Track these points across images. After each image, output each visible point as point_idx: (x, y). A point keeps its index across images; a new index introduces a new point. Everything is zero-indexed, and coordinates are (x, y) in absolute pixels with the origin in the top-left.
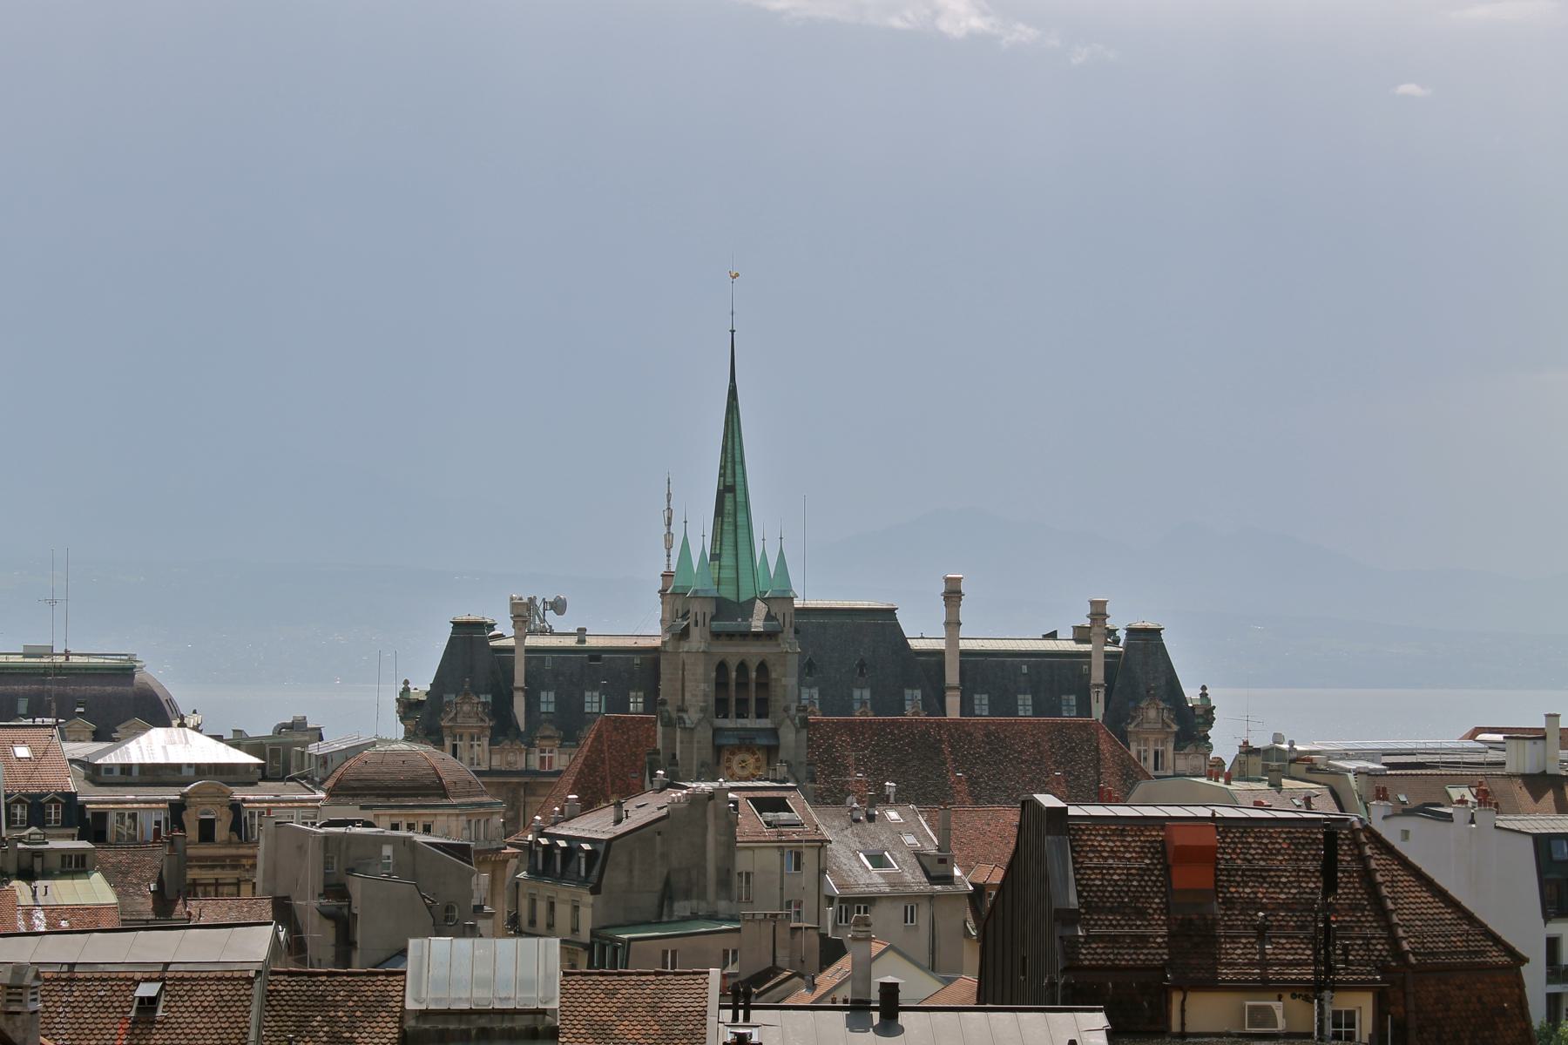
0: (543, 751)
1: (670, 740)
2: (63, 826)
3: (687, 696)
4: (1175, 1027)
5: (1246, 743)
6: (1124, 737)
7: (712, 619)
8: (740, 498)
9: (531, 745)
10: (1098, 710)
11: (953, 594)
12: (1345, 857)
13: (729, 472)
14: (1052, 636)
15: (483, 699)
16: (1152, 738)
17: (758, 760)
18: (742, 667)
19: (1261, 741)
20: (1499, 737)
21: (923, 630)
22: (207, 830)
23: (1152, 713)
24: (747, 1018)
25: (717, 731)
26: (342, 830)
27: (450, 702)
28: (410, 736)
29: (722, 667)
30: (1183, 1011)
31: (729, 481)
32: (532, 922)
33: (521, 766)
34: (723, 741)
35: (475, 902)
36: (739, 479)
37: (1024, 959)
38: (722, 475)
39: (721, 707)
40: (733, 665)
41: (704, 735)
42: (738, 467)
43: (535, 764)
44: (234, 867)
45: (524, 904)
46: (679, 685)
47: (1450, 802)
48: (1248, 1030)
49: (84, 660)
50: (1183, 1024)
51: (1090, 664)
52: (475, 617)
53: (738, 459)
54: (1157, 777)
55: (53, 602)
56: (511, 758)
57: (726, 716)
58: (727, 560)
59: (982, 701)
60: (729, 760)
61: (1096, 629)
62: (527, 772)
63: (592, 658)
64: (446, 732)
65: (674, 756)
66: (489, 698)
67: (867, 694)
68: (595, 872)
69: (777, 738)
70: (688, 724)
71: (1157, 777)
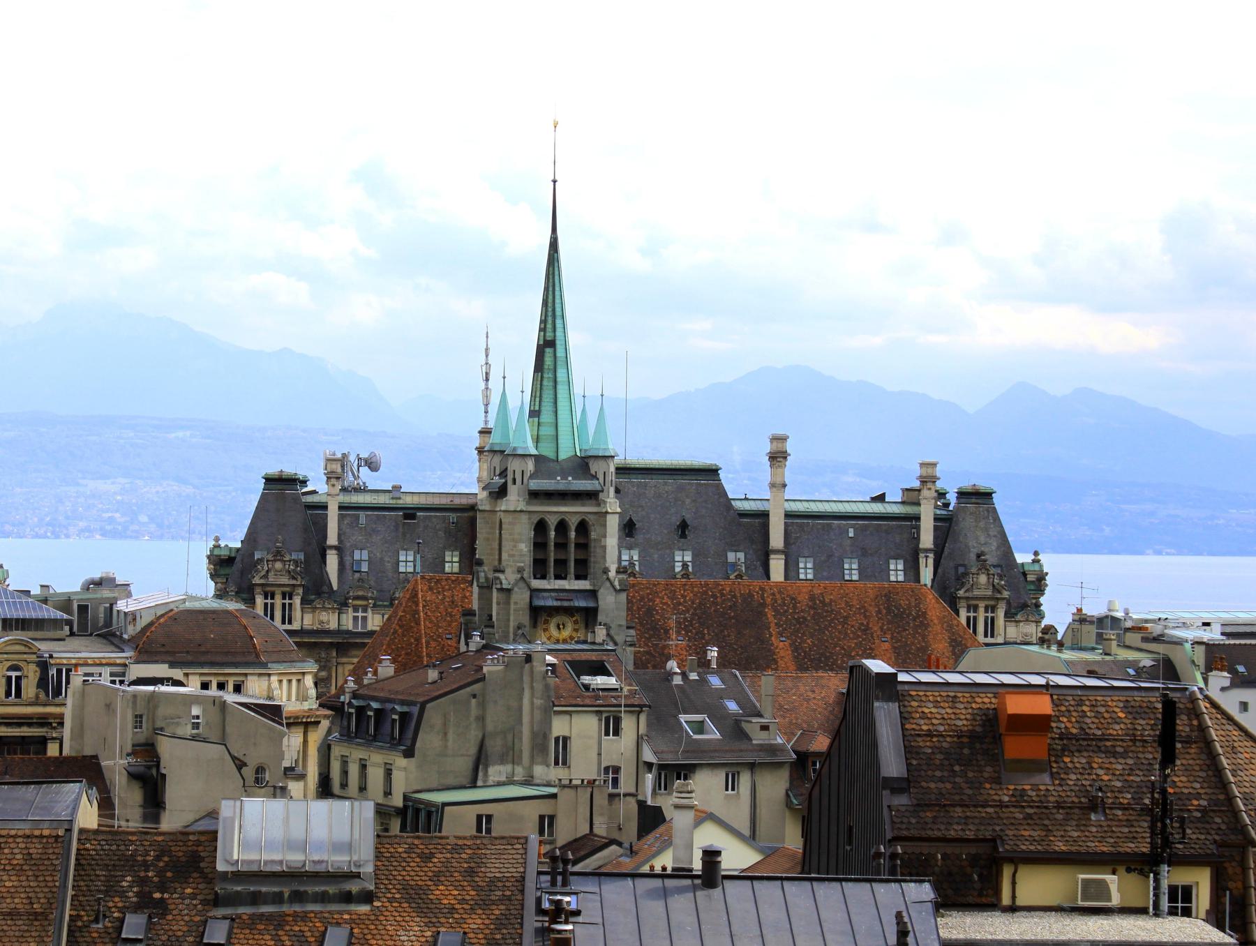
3: (505, 556)
5: (1079, 610)
7: (531, 477)
8: (560, 353)
10: (927, 575)
17: (576, 622)
18: (562, 526)
19: (1094, 609)
21: (745, 484)
24: (565, 884)
26: (151, 688)
28: (220, 595)
29: (541, 527)
30: (1014, 883)
31: (549, 335)
32: (344, 785)
33: (333, 625)
34: (541, 603)
35: (286, 763)
36: (559, 333)
37: (850, 828)
38: (543, 329)
39: (540, 568)
40: (552, 522)
41: (521, 598)
43: (348, 622)
44: (42, 725)
46: (496, 546)
48: (1080, 903)
50: (1014, 897)
51: (918, 528)
52: (289, 469)
53: (558, 313)
56: (324, 616)
57: (543, 577)
58: (546, 416)
59: (806, 570)
60: (546, 622)
61: (925, 493)
62: (338, 632)
63: (407, 516)
64: (258, 590)
65: (490, 616)
66: (302, 557)
68: (410, 734)
71: (987, 645)
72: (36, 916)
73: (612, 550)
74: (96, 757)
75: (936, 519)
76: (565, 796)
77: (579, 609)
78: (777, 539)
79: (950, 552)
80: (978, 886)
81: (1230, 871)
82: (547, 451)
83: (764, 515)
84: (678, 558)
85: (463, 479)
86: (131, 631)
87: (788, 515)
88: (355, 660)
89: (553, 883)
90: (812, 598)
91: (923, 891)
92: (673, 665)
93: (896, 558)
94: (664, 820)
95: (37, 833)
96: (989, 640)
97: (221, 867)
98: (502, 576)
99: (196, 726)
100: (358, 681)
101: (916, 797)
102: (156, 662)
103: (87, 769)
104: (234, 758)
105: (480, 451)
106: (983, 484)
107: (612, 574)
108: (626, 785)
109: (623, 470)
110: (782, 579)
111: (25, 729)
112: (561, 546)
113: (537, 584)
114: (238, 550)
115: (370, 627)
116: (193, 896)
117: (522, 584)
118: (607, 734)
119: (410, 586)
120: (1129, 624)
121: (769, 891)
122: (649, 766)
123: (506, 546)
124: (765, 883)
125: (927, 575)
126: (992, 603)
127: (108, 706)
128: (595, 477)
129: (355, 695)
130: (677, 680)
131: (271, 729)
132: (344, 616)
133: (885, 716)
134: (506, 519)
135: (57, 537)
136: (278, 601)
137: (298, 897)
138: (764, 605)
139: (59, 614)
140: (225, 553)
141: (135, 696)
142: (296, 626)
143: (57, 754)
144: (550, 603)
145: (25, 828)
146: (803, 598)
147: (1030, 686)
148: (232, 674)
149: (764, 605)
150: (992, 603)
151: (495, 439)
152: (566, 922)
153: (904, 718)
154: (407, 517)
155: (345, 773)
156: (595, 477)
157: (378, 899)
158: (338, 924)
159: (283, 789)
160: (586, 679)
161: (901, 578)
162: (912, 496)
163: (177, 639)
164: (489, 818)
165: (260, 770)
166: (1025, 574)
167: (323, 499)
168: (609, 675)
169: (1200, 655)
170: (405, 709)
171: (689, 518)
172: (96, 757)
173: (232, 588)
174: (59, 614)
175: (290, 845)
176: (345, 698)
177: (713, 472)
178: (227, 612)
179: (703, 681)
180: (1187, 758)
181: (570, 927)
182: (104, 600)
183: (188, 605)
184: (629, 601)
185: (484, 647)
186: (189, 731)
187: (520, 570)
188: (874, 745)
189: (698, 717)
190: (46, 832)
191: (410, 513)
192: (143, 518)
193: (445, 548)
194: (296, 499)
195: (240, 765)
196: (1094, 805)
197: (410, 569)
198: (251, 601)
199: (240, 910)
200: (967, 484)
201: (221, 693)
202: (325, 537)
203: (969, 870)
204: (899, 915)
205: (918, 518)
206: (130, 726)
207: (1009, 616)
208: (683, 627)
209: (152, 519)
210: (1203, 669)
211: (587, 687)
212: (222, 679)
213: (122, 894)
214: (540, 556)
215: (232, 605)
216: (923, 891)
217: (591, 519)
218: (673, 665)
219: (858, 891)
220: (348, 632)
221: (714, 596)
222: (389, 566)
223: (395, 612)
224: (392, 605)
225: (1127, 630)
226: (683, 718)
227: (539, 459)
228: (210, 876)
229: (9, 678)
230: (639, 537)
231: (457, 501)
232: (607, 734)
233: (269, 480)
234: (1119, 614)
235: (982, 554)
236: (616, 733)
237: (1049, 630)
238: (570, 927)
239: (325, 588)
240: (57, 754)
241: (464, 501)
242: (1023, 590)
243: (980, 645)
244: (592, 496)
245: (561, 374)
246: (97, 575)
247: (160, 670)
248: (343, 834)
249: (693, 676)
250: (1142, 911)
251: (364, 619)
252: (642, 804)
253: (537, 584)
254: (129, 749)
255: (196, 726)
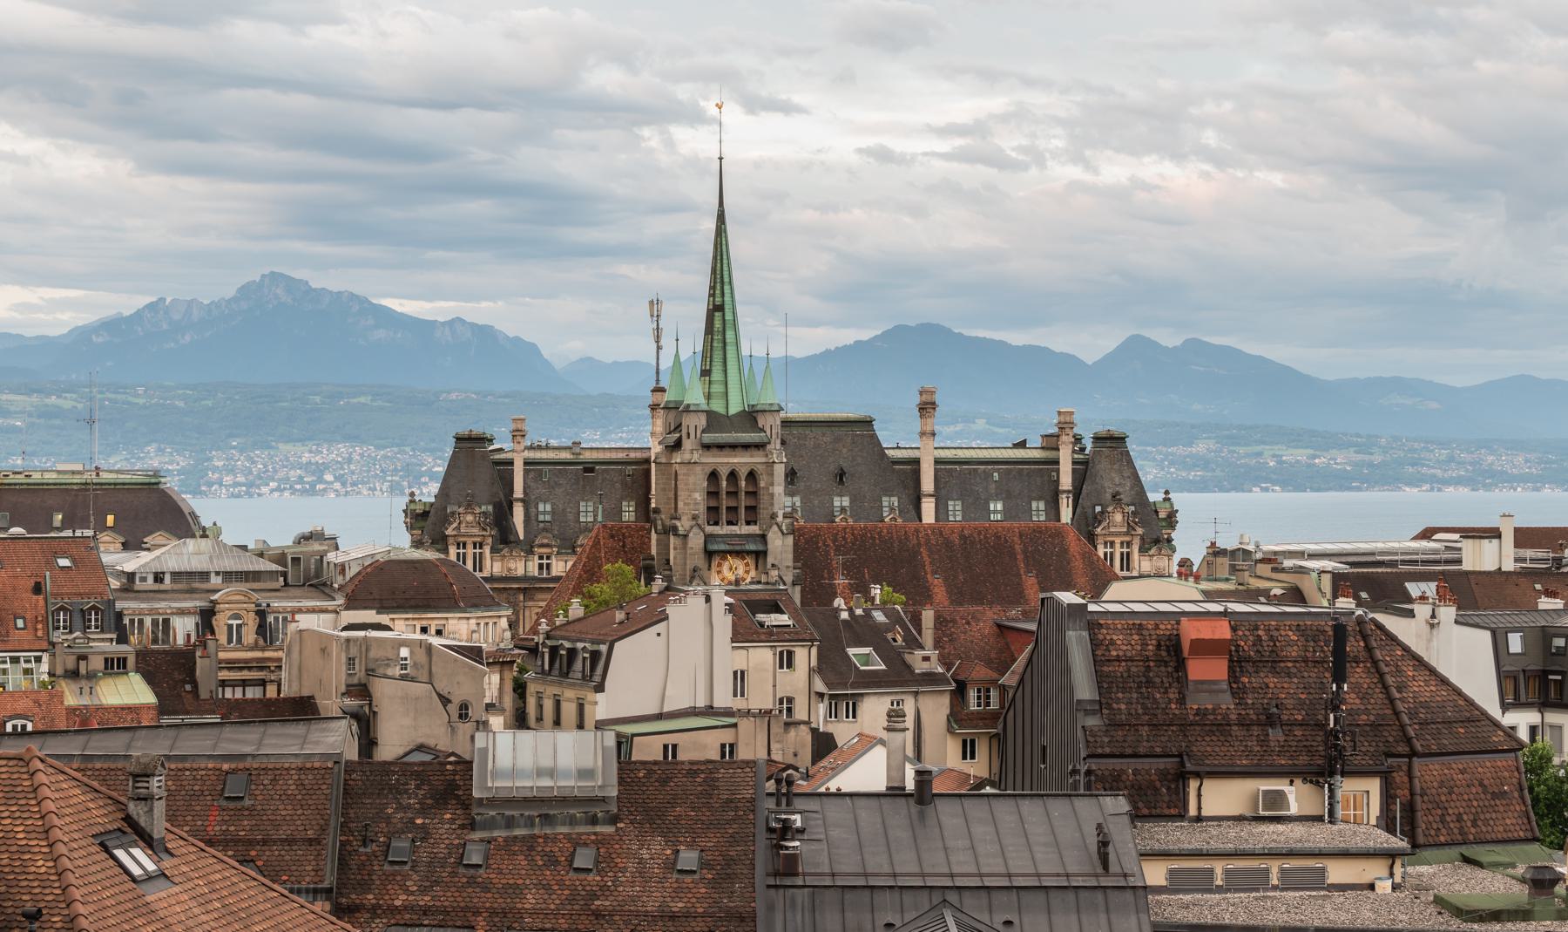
0: (541, 558)
1: (664, 547)
2: (102, 631)
3: (680, 505)
4: (1193, 812)
5: (1213, 544)
6: (1092, 538)
7: (703, 431)
8: (729, 317)
9: (530, 552)
10: (1066, 514)
11: (927, 407)
12: (1354, 646)
13: (718, 292)
14: (1022, 445)
15: (484, 508)
16: (1118, 541)
17: (747, 565)
18: (733, 475)
19: (1228, 542)
20: (1456, 536)
21: (898, 435)
22: (235, 634)
23: (1118, 517)
24: (788, 804)
25: (708, 538)
26: (361, 634)
27: (453, 513)
28: (417, 544)
29: (713, 476)
30: (1199, 796)
31: (718, 300)
32: (540, 719)
33: (520, 572)
34: (715, 547)
35: (487, 700)
36: (727, 298)
37: (1044, 748)
38: (712, 295)
39: (713, 514)
40: (724, 473)
41: (696, 541)
42: (727, 288)
43: (533, 569)
44: (261, 668)
45: (531, 702)
46: (672, 495)
47: (1410, 600)
48: (1262, 813)
49: (113, 476)
50: (1199, 808)
51: (1058, 471)
52: (478, 429)
53: (726, 279)
54: (1125, 578)
55: (91, 422)
56: (512, 565)
57: (716, 523)
58: (717, 375)
59: (955, 509)
60: (720, 565)
61: (1064, 438)
62: (525, 578)
63: (587, 470)
64: (451, 540)
65: (668, 561)
66: (490, 508)
67: (846, 502)
68: (599, 670)
69: (765, 543)
70: (681, 531)
71: (1125, 578)
72: (310, 841)
73: (781, 500)
74: (312, 697)
75: (1074, 463)
76: (745, 725)
77: (749, 553)
78: (928, 484)
79: (1098, 489)
80: (1166, 798)
81: (1398, 780)
82: (717, 406)
83: (916, 462)
84: (837, 504)
85: (641, 435)
86: (338, 581)
87: (937, 462)
88: (543, 604)
89: (778, 804)
90: (963, 537)
91: (1118, 804)
92: (839, 602)
93: (1039, 499)
94: (836, 747)
95: (308, 765)
96: (1125, 573)
97: (476, 794)
98: (678, 523)
99: (404, 667)
100: (551, 622)
101: (1157, 719)
102: (365, 608)
103: (303, 709)
104: (440, 695)
105: (654, 407)
106: (1116, 429)
107: (780, 519)
108: (800, 713)
109: (786, 423)
110: (932, 521)
111: (245, 672)
112: (733, 494)
113: (710, 529)
114: (432, 505)
115: (555, 572)
116: (452, 821)
117: (695, 530)
118: (781, 667)
119: (593, 534)
120: (1259, 556)
121: (976, 809)
122: (821, 695)
123: (682, 494)
124: (946, 800)
125: (1066, 514)
126: (1127, 539)
127: (323, 650)
128: (762, 430)
129: (548, 636)
130: (845, 615)
131: (473, 668)
132: (530, 564)
133: (1076, 642)
134: (681, 471)
135: (251, 496)
136: (470, 551)
137: (547, 819)
138: (919, 545)
139: (275, 567)
140: (419, 509)
141: (348, 640)
142: (486, 574)
143: (275, 695)
144: (723, 547)
145: (299, 762)
146: (955, 539)
147: (1208, 613)
148: (434, 619)
149: (919, 545)
150: (1127, 539)
151: (669, 396)
152: (793, 840)
153: (1095, 644)
154: (586, 472)
155: (540, 707)
156: (762, 430)
157: (621, 821)
158: (586, 845)
159: (486, 723)
160: (761, 617)
161: (1042, 518)
162: (1051, 443)
163: (386, 587)
164: (675, 747)
165: (464, 707)
166: (1157, 512)
167: (509, 456)
168: (782, 612)
169: (1327, 582)
170: (595, 647)
171: (845, 466)
172: (312, 697)
173: (426, 538)
174: (275, 567)
175: (540, 773)
176: (539, 639)
177: (867, 423)
178: (428, 561)
179: (867, 612)
180: (1358, 675)
181: (797, 843)
182: (314, 553)
183: (393, 556)
184: (795, 544)
185: (667, 589)
186: (397, 672)
187: (695, 518)
188: (1067, 671)
189: (866, 650)
190: (317, 765)
191: (589, 468)
192: (329, 477)
193: (622, 499)
194: (485, 455)
195: (445, 701)
196: (1270, 721)
197: (590, 519)
198: (446, 551)
199: (496, 834)
200: (1101, 429)
201: (424, 637)
202: (512, 491)
203: (1158, 784)
204: (1099, 826)
205: (1057, 462)
206: (344, 668)
207: (1143, 550)
208: (848, 569)
209: (337, 479)
210: (1329, 595)
211: (762, 625)
212: (425, 623)
213: (388, 820)
214: (713, 504)
215: (430, 555)
216: (1118, 804)
217: (760, 469)
218: (839, 602)
219: (1058, 807)
220: (534, 579)
221: (873, 538)
222: (571, 516)
223: (580, 559)
224: (574, 552)
225: (1257, 561)
226: (851, 651)
227: (710, 414)
228: (466, 803)
229: (230, 627)
230: (801, 485)
231: (633, 455)
232: (781, 667)
233: (459, 439)
234: (1251, 548)
235: (1118, 493)
236: (790, 665)
237: (1185, 563)
238: (797, 843)
239: (512, 538)
240: (275, 695)
241: (639, 455)
242: (1155, 528)
243: (1117, 578)
244: (760, 446)
245: (730, 335)
246: (307, 529)
247: (369, 616)
248: (588, 762)
249: (859, 612)
250: (1320, 819)
251: (548, 565)
252: (815, 731)
253: (710, 529)
254: (343, 689)
255: (404, 667)
